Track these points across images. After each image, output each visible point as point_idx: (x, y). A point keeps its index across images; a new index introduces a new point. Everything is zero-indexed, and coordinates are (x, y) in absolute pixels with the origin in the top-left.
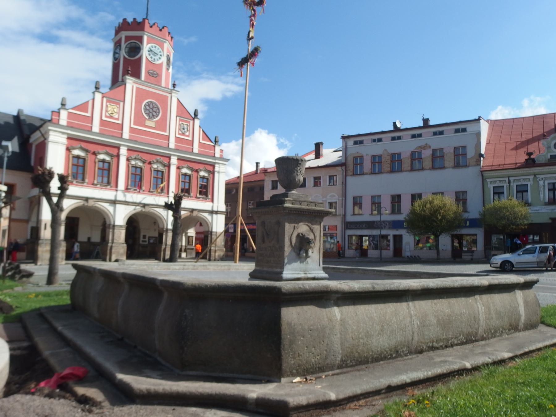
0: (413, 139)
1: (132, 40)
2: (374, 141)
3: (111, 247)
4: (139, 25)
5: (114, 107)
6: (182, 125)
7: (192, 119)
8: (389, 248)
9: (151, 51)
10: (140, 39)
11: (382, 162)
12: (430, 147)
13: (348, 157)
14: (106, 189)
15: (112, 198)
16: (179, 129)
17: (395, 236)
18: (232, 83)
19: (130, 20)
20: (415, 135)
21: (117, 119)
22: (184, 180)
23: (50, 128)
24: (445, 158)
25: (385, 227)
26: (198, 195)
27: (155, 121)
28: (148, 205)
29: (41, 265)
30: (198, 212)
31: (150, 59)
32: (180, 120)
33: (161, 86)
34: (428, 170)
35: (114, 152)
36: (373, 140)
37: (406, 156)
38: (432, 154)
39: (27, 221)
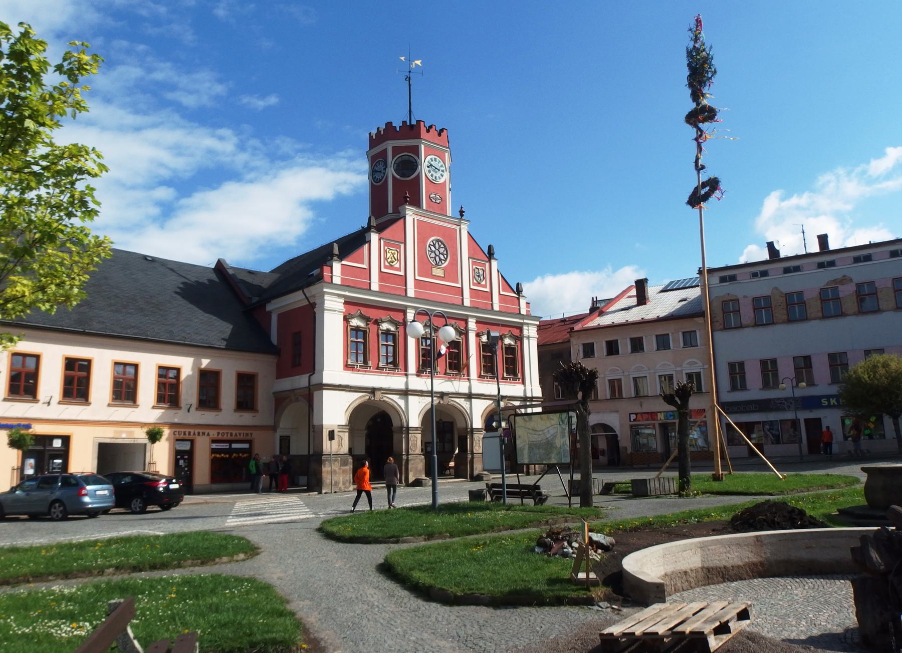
0: (821, 270)
1: (403, 152)
2: (755, 275)
3: (407, 460)
4: (412, 130)
5: (393, 252)
6: (477, 271)
7: (487, 260)
8: (57, 443)
9: (431, 165)
10: (416, 150)
11: (771, 307)
12: (851, 280)
13: (712, 301)
14: (365, 371)
15: (402, 387)
16: (474, 277)
17: (807, 421)
18: (347, 170)
19: (397, 124)
20: (824, 263)
21: (399, 269)
22: (385, 343)
23: (325, 290)
24: (879, 297)
25: (789, 407)
26: (448, 371)
27: (444, 267)
28: (447, 394)
29: (325, 493)
30: (508, 400)
31: (430, 178)
32: (474, 263)
33: (446, 216)
34: (853, 315)
35: (399, 317)
36: (752, 274)
37: (812, 294)
38: (856, 291)
39: (274, 428)
